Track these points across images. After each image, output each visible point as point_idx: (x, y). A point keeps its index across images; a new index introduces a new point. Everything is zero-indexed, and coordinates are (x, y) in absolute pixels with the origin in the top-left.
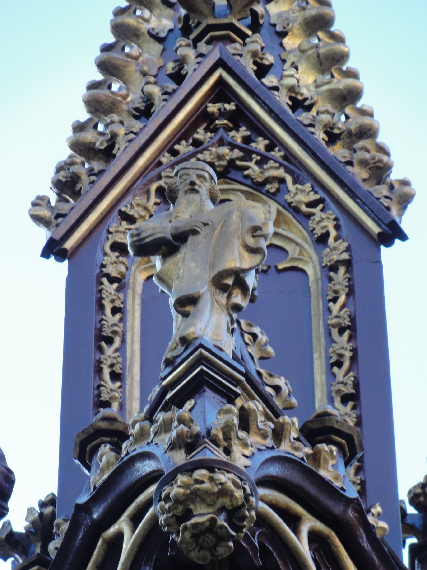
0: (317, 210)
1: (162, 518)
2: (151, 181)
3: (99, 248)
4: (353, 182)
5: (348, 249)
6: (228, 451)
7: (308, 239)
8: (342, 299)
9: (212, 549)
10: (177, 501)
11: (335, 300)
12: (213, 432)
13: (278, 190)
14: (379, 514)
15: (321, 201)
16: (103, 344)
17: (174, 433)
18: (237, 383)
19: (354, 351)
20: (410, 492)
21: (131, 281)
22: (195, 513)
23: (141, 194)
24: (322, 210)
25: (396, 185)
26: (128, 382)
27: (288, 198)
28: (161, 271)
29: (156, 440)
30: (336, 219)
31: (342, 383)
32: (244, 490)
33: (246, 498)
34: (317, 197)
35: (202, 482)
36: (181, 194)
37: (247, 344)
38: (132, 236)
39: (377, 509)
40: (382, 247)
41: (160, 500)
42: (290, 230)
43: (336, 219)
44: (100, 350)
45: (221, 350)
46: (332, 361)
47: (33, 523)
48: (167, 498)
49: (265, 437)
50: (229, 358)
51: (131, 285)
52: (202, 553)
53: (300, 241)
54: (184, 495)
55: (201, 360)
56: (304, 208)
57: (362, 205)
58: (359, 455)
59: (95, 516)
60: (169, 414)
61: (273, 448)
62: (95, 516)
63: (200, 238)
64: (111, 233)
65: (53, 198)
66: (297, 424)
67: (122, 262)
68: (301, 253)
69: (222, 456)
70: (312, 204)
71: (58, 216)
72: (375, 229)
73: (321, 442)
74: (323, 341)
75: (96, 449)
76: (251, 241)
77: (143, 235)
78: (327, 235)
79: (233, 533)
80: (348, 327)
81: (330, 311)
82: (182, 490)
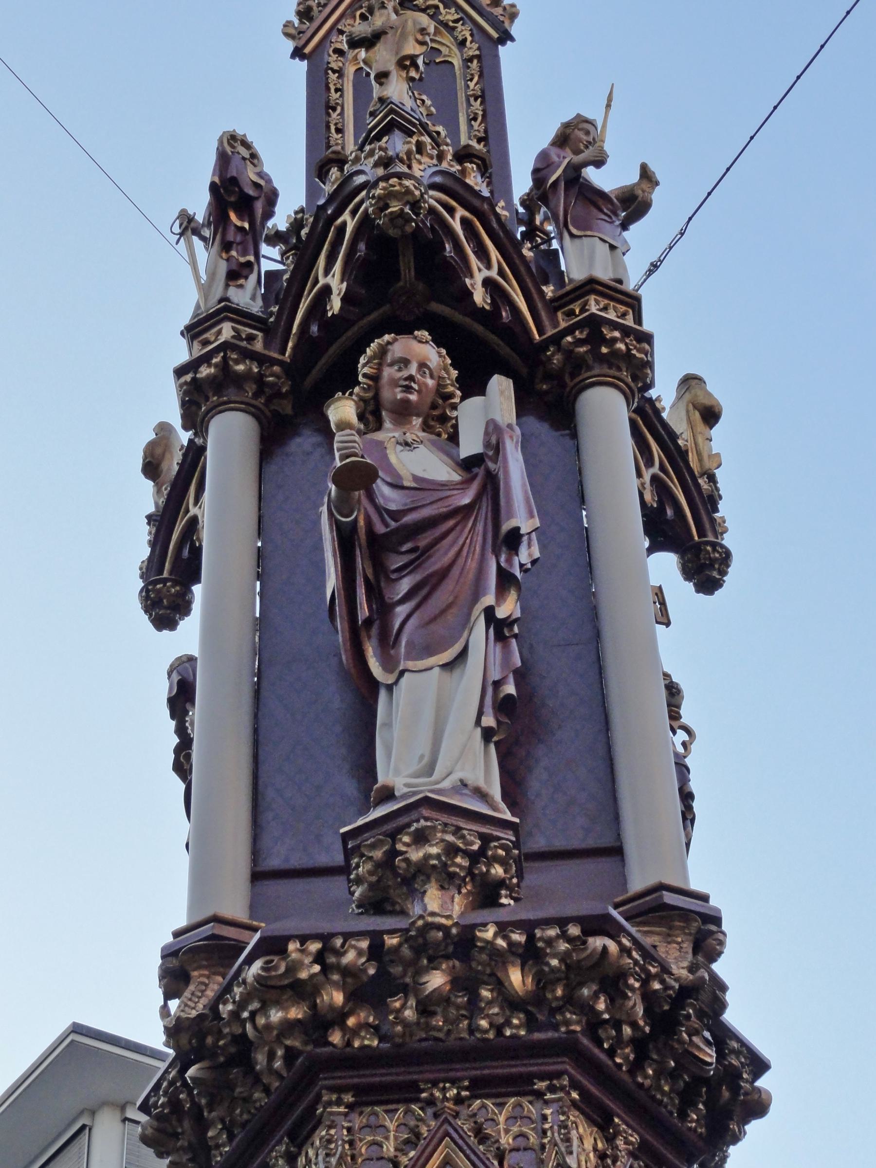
0: (459, 25)
1: (370, 210)
2: (357, 10)
3: (326, 53)
4: (481, 6)
5: (479, 49)
6: (410, 167)
7: (454, 43)
8: (476, 79)
9: (402, 228)
10: (380, 198)
11: (471, 80)
12: (401, 155)
13: (435, 13)
14: (503, 207)
15: (461, 19)
16: (330, 111)
17: (376, 157)
18: (414, 125)
19: (484, 111)
20: (520, 198)
21: (346, 72)
22: (391, 205)
23: (351, 18)
24: (462, 25)
25: (508, 8)
26: (346, 134)
27: (441, 18)
28: (365, 58)
29: (366, 162)
30: (471, 30)
31: (478, 130)
32: (421, 190)
33: (422, 195)
34: (459, 16)
35: (394, 186)
36: (376, 10)
37: (419, 106)
38: (346, 36)
39: (502, 204)
40: (499, 46)
41: (369, 198)
42: (442, 37)
43: (471, 30)
44: (329, 115)
45: (404, 105)
46: (471, 117)
47: (291, 224)
48: (373, 197)
49: (432, 158)
50: (409, 110)
51: (346, 75)
52: (395, 231)
53: (449, 44)
54: (384, 194)
55: (392, 111)
56: (451, 24)
57: (487, 20)
58: (489, 171)
59: (329, 212)
60: (373, 145)
61: (437, 165)
62: (329, 212)
63: (389, 36)
64: (333, 43)
65: (296, 22)
66: (451, 151)
67: (340, 61)
68: (450, 52)
69: (405, 169)
70: (456, 21)
71: (300, 33)
72: (495, 35)
73: (467, 162)
74: (465, 105)
75: (329, 170)
76: (420, 37)
77: (353, 36)
78: (465, 40)
79: (415, 217)
80: (480, 96)
81: (468, 87)
82: (382, 192)
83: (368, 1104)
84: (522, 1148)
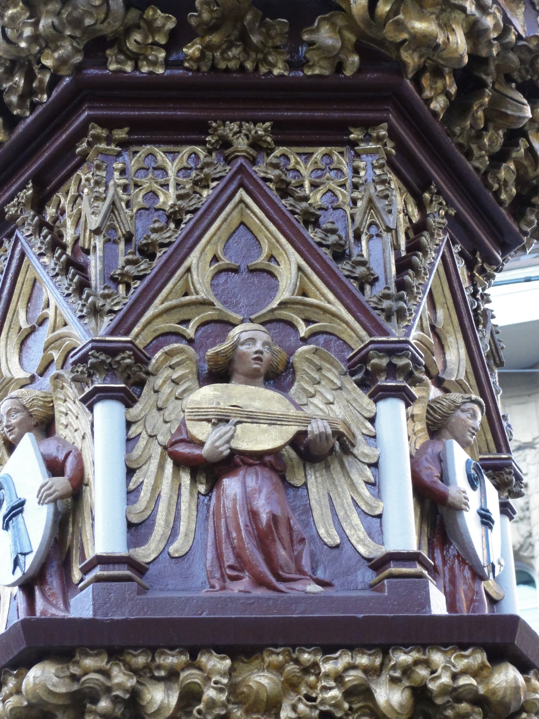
83: (141, 143)
84: (375, 237)
